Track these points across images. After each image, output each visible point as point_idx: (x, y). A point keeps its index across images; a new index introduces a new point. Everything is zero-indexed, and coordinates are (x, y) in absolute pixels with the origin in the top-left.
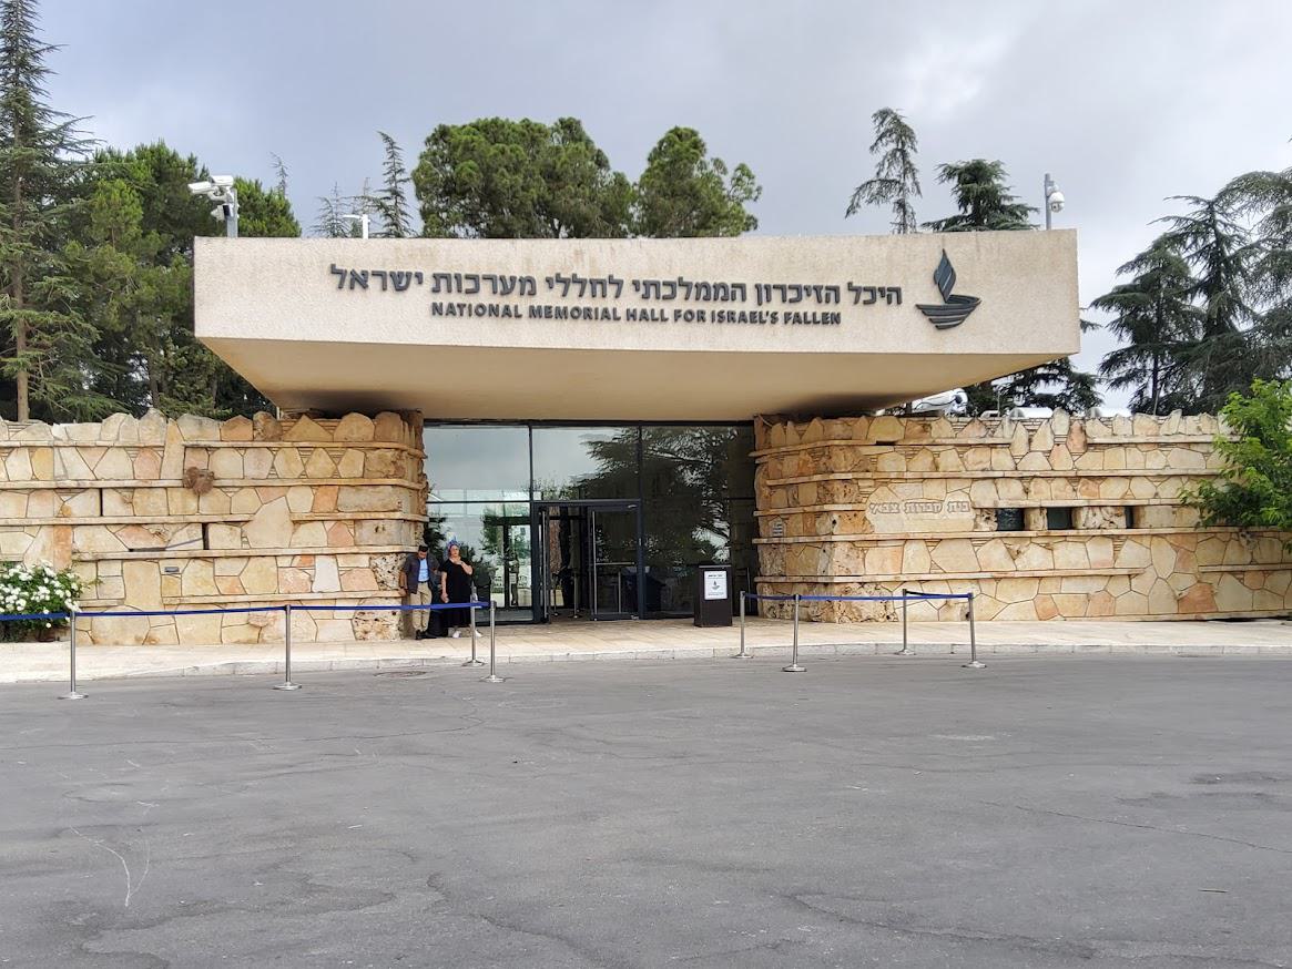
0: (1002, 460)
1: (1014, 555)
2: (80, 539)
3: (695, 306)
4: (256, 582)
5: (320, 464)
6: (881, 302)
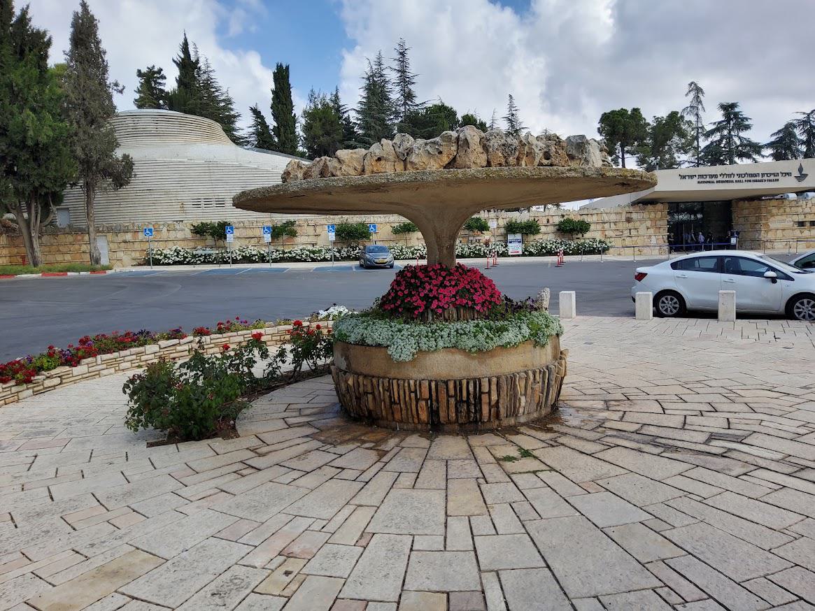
0: (800, 210)
1: (802, 232)
3: (749, 179)
4: (640, 242)
5: (653, 215)
6: (787, 176)
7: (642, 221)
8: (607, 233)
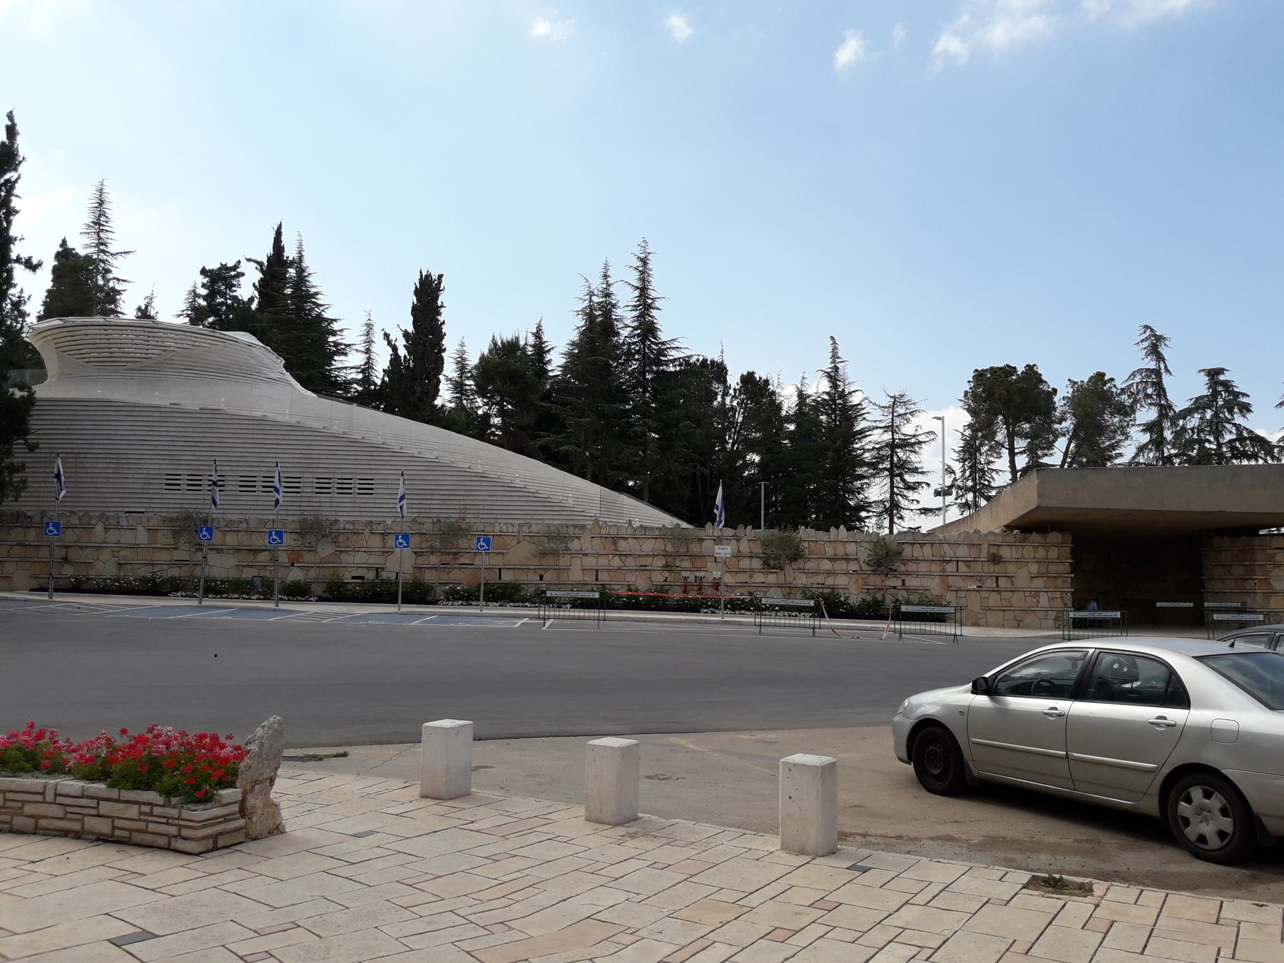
2: (951, 580)
5: (1041, 553)
7: (1019, 562)
8: (951, 580)
